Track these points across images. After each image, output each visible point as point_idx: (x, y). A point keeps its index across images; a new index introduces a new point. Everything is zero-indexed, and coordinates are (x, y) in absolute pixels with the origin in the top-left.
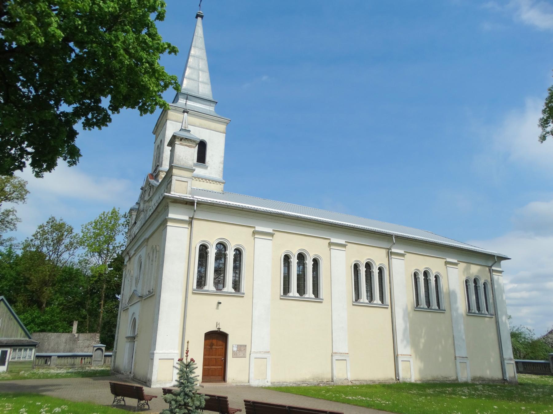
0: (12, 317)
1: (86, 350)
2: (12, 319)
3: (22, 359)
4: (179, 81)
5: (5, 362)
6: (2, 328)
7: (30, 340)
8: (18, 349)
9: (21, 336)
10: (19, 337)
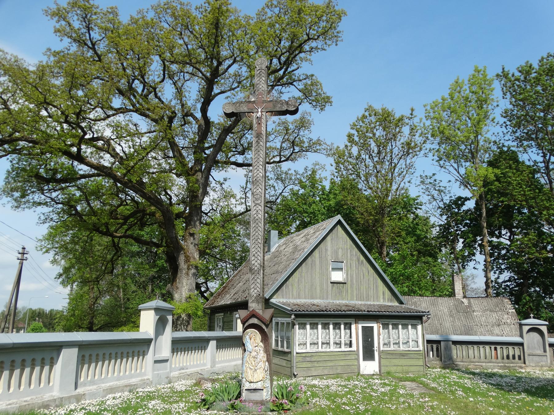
0: (362, 258)
1: (497, 330)
2: (362, 262)
3: (402, 348)
4: (211, 409)
5: (373, 351)
6: (349, 279)
7: (403, 306)
8: (320, 323)
9: (384, 298)
10: (382, 301)
